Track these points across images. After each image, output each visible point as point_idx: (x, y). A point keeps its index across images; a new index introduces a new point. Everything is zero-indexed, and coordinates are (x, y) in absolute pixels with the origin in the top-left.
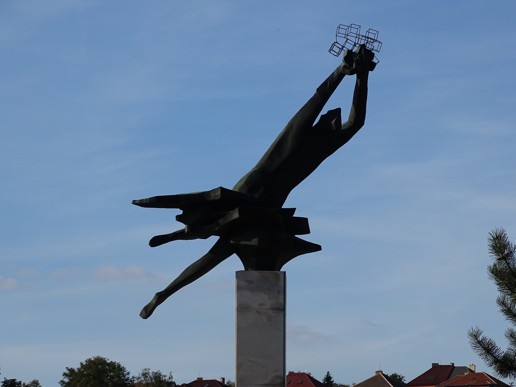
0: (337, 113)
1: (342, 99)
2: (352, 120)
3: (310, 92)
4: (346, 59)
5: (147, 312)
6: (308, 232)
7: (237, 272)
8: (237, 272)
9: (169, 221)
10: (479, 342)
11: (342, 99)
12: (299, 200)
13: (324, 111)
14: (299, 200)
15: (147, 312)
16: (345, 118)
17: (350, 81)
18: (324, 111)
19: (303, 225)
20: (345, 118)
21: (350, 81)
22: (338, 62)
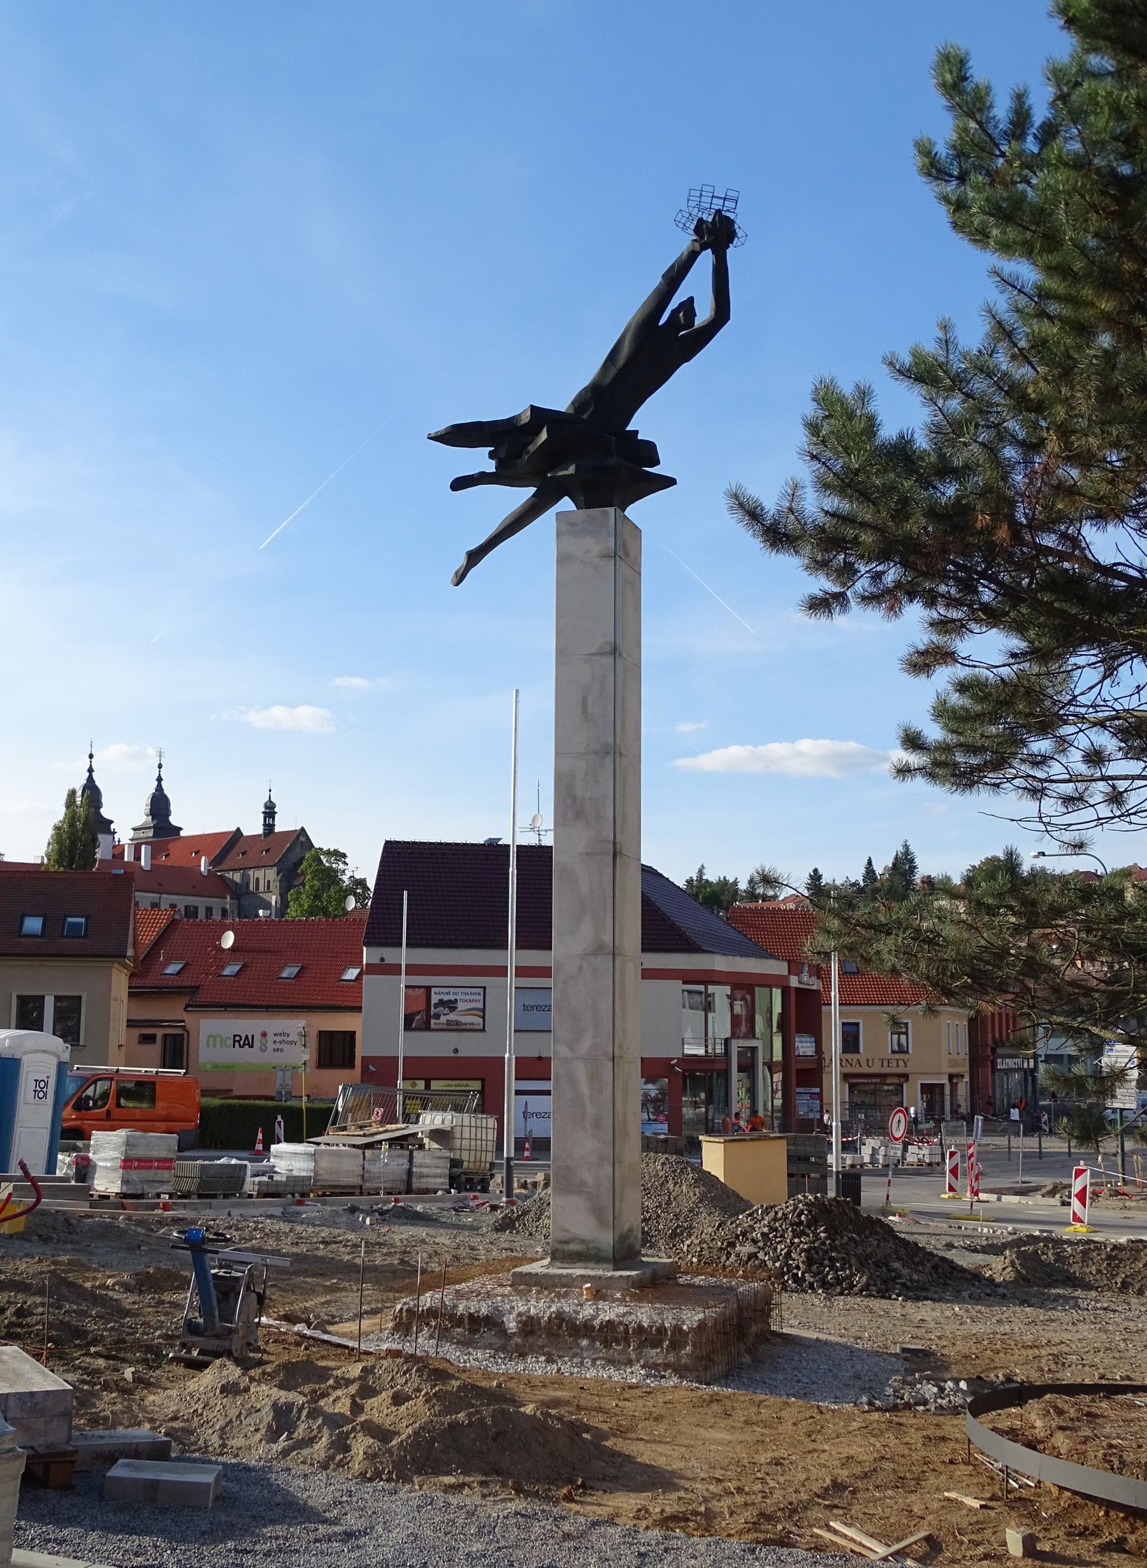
0: (688, 306)
1: (697, 286)
2: (713, 313)
3: (655, 281)
4: (696, 231)
5: (460, 578)
6: (658, 463)
7: (387, 842)
8: (387, 842)
9: (480, 460)
10: (898, 371)
11: (697, 286)
12: (645, 422)
13: (673, 304)
14: (645, 422)
15: (460, 578)
16: (704, 313)
17: (706, 259)
18: (673, 304)
19: (649, 452)
20: (704, 313)
21: (706, 259)
22: (685, 240)
